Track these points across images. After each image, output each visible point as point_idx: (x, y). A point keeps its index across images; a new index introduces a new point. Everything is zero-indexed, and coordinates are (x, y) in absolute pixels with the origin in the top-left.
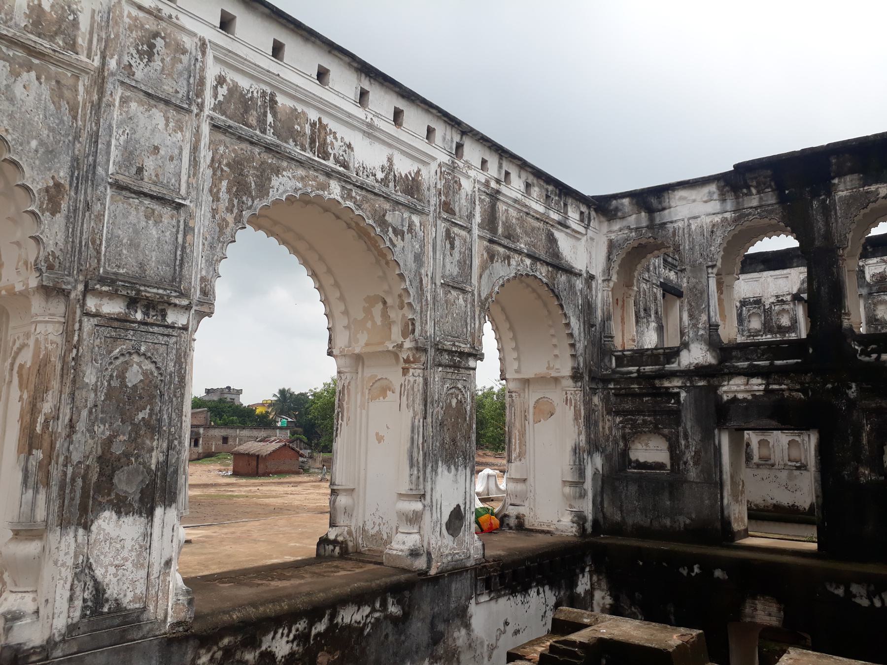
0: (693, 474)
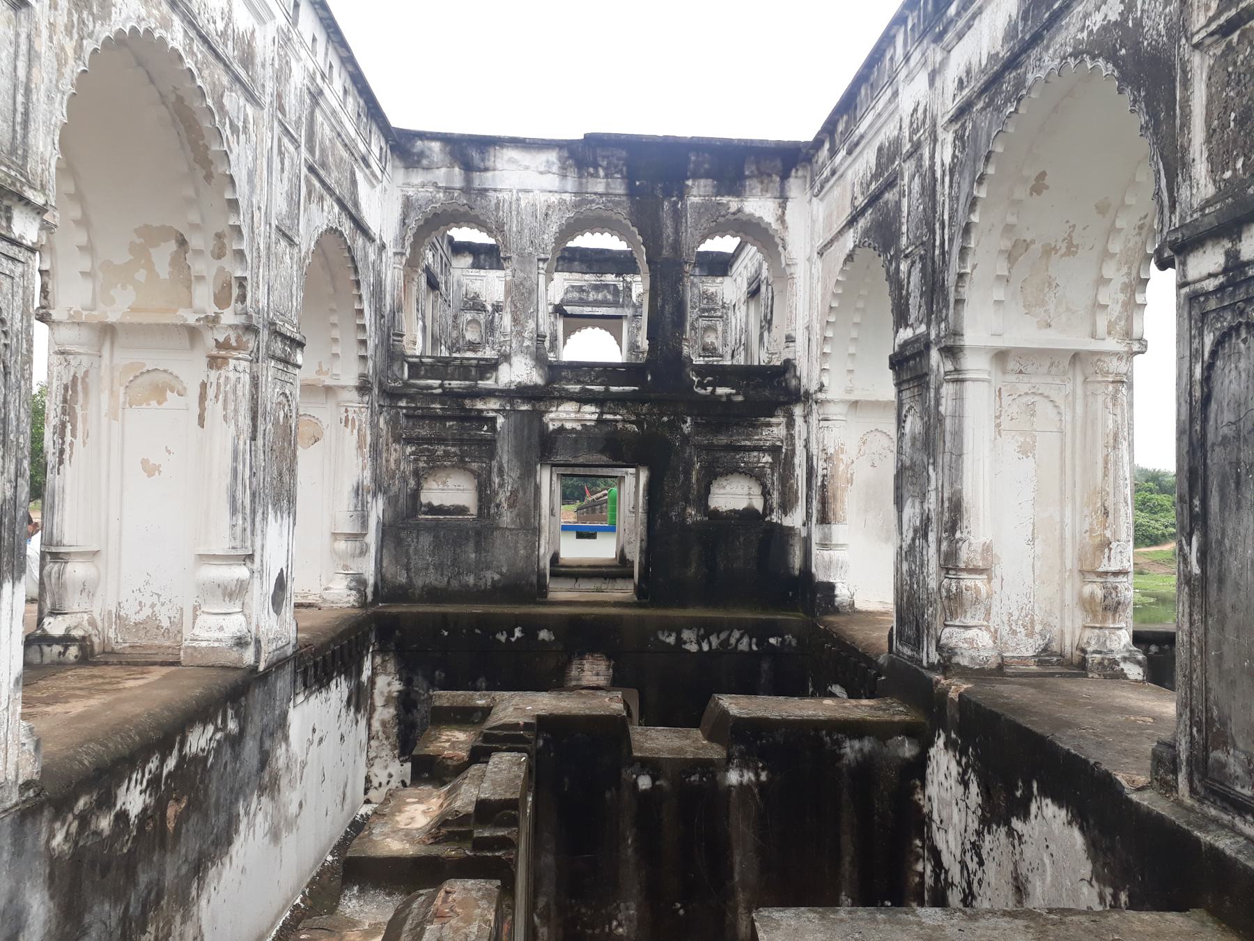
0: (507, 518)
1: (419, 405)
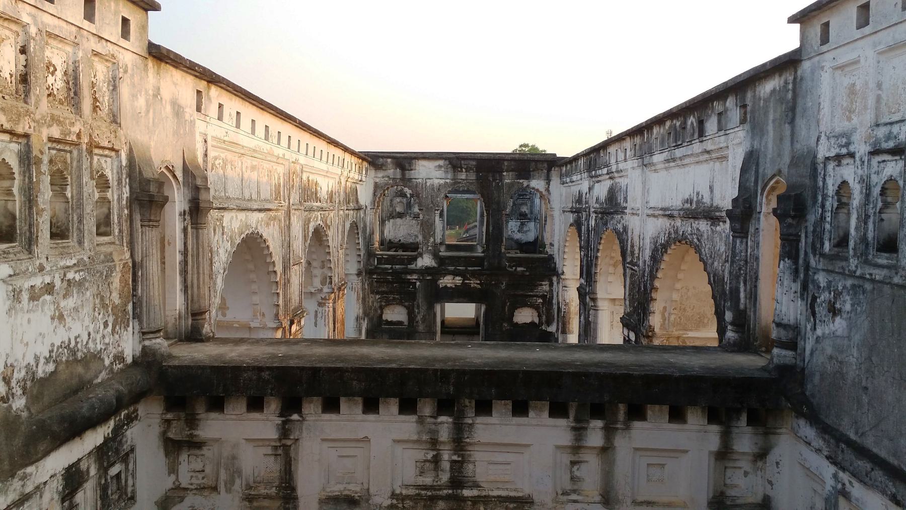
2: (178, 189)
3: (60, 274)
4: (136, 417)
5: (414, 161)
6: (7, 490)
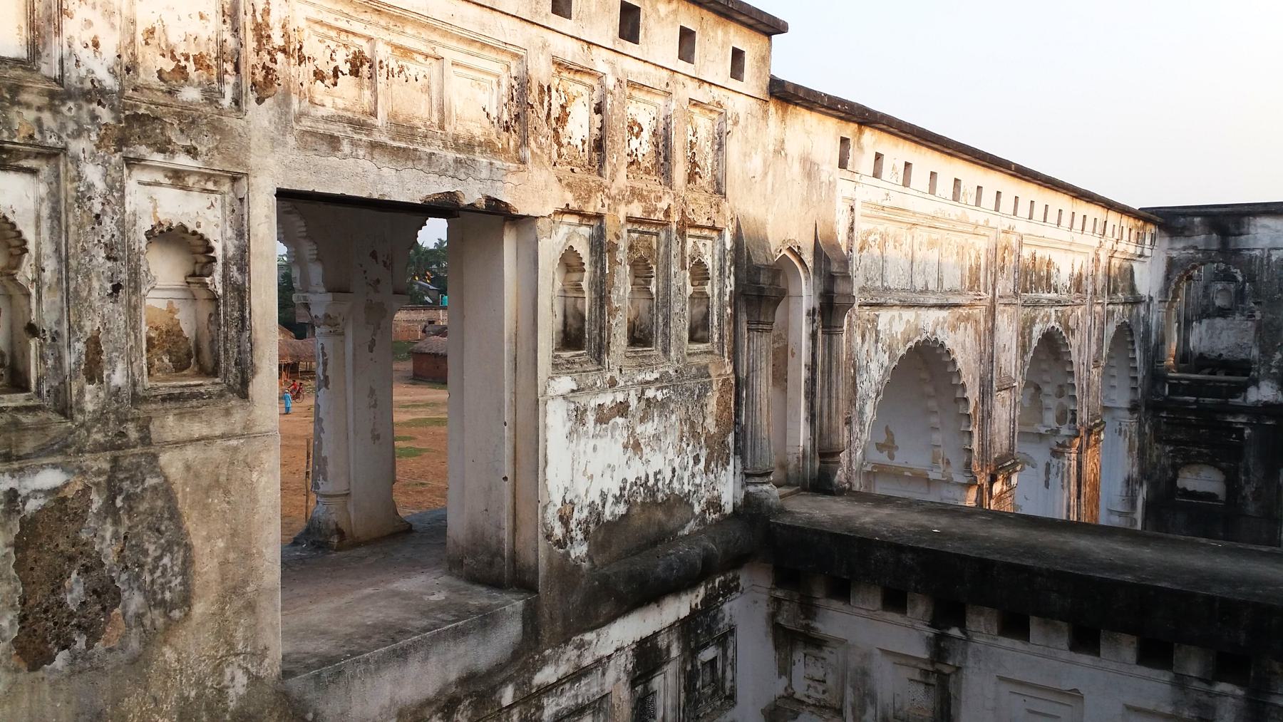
0: (1252, 508)
1: (1177, 416)
2: (806, 279)
3: (636, 390)
4: (737, 588)
5: (1246, 220)
6: (559, 658)
